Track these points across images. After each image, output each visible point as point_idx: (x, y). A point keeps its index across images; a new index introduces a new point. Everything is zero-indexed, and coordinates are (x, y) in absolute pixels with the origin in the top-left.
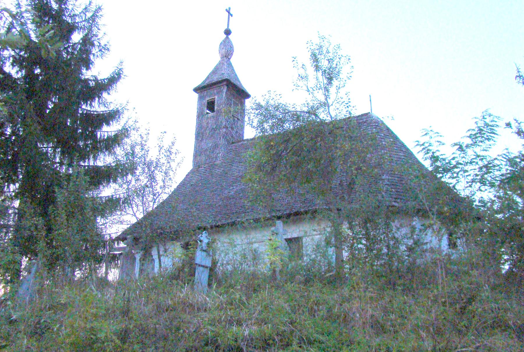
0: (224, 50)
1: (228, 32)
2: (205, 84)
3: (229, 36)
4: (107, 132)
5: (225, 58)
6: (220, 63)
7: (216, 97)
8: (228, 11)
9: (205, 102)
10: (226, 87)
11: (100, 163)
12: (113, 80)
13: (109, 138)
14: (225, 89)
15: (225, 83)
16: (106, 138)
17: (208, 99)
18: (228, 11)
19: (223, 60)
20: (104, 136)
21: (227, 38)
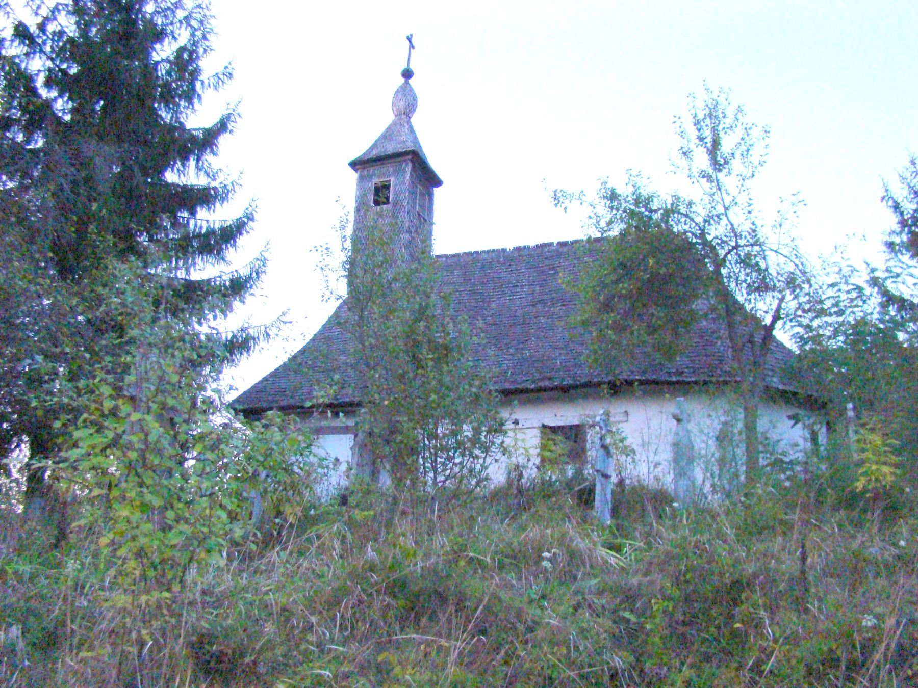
0: (402, 103)
1: (407, 74)
2: (374, 153)
3: (410, 81)
4: (207, 221)
5: (403, 117)
6: (394, 124)
7: (392, 179)
8: (409, 39)
9: (371, 186)
10: (410, 165)
11: (196, 275)
12: (222, 126)
13: (211, 233)
14: (409, 168)
15: (410, 157)
16: (203, 231)
17: (376, 180)
18: (409, 39)
19: (400, 119)
20: (201, 228)
21: (407, 83)
